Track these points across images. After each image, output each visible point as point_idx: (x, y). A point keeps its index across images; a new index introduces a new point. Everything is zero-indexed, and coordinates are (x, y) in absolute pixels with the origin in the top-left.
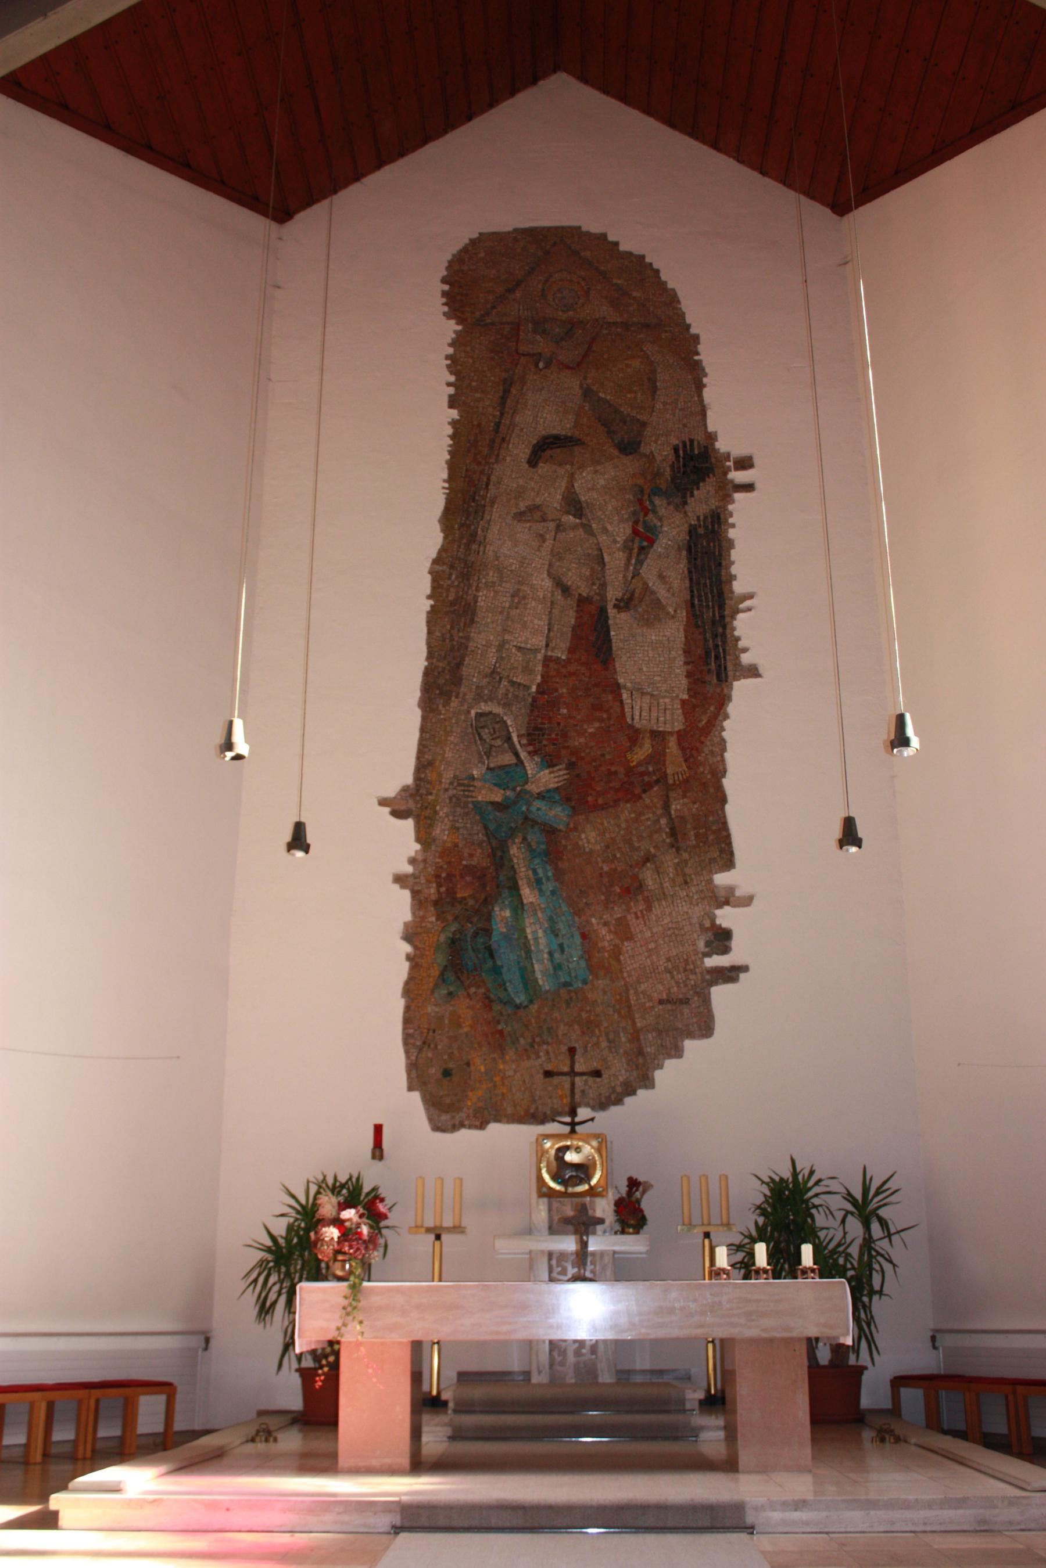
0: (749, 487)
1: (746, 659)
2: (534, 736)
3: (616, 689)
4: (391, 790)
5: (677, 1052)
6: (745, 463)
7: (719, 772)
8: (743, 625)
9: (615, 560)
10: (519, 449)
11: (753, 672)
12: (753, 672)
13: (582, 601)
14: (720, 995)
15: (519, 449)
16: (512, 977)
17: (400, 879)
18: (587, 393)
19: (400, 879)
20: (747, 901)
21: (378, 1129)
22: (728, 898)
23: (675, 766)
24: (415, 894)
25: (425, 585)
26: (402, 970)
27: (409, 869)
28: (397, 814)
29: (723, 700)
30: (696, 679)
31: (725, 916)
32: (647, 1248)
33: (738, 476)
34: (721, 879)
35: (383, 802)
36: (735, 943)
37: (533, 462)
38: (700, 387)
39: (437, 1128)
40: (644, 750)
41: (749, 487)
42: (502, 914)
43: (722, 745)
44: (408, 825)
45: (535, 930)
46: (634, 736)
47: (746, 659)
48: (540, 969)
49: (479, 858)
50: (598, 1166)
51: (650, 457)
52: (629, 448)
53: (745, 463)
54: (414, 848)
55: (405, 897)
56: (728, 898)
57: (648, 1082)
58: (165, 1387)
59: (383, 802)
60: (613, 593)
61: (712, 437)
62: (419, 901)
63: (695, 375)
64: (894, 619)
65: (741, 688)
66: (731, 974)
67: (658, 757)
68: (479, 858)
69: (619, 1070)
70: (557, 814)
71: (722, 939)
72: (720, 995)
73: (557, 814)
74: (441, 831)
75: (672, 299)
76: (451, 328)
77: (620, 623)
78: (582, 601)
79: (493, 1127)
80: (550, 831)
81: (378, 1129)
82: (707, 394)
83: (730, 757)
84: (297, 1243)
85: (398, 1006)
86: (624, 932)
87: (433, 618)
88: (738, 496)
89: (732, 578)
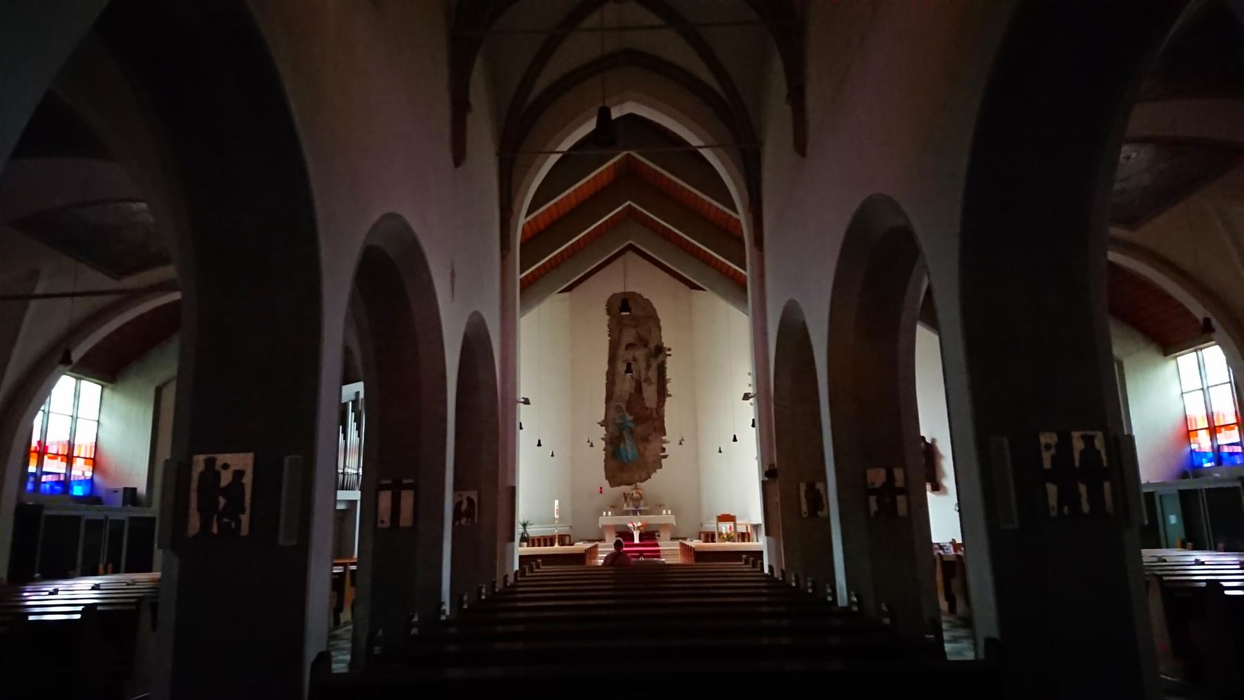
0: (670, 355)
1: (669, 393)
2: (627, 409)
3: (643, 399)
4: (600, 421)
5: (655, 471)
6: (669, 350)
7: (663, 417)
8: (669, 386)
9: (643, 372)
10: (623, 347)
11: (670, 396)
12: (670, 396)
13: (637, 381)
14: (663, 461)
15: (623, 347)
16: (624, 458)
17: (603, 439)
18: (637, 333)
19: (603, 439)
20: (668, 442)
21: (601, 488)
22: (665, 442)
23: (655, 415)
24: (606, 442)
25: (605, 377)
26: (604, 457)
27: (604, 437)
28: (602, 426)
29: (664, 401)
30: (659, 398)
31: (665, 445)
32: (631, 459)
33: (668, 353)
34: (664, 438)
35: (599, 423)
36: (666, 451)
37: (626, 349)
38: (660, 331)
39: (611, 486)
40: (648, 412)
41: (670, 355)
42: (622, 445)
43: (664, 411)
44: (604, 428)
45: (629, 448)
46: (647, 409)
47: (669, 393)
48: (630, 456)
49: (617, 434)
50: (194, 485)
51: (650, 349)
52: (646, 346)
53: (669, 350)
54: (605, 432)
55: (604, 442)
56: (665, 442)
57: (650, 478)
58: (569, 536)
59: (599, 423)
60: (642, 379)
61: (663, 344)
62: (606, 444)
63: (660, 328)
65: (668, 399)
66: (665, 457)
67: (652, 413)
68: (617, 434)
69: (644, 475)
70: (632, 425)
71: (663, 450)
72: (663, 461)
73: (632, 425)
74: (610, 429)
75: (654, 310)
76: (608, 317)
77: (644, 385)
78: (637, 381)
79: (607, 481)
80: (631, 429)
81: (601, 488)
82: (662, 333)
83: (666, 413)
85: (603, 464)
86: (645, 448)
87: (607, 384)
88: (668, 357)
89: (666, 376)
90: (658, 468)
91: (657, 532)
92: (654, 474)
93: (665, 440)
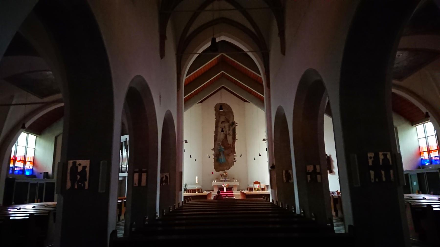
0: (237, 125)
1: (237, 139)
2: (222, 144)
3: (228, 141)
4: (212, 149)
5: (232, 166)
6: (237, 123)
7: (235, 147)
8: (237, 136)
9: (227, 131)
10: (220, 122)
11: (237, 140)
12: (237, 140)
13: (225, 134)
14: (235, 163)
15: (220, 122)
16: (221, 162)
17: (213, 155)
18: (225, 118)
19: (213, 155)
20: (236, 156)
21: (213, 172)
22: (235, 156)
23: (232, 147)
24: (214, 156)
25: (214, 133)
26: (214, 161)
27: (214, 154)
28: (213, 150)
29: (235, 142)
30: (233, 140)
31: (235, 157)
33: (236, 124)
34: (235, 155)
35: (212, 149)
36: (236, 159)
37: (221, 123)
38: (234, 117)
39: (216, 172)
40: (229, 145)
41: (237, 125)
42: (220, 157)
43: (235, 145)
44: (214, 151)
45: (222, 158)
46: (229, 144)
47: (237, 139)
48: (223, 161)
49: (218, 153)
51: (230, 123)
52: (228, 122)
53: (237, 123)
54: (214, 153)
55: (214, 156)
56: (235, 156)
57: (230, 168)
58: (201, 189)
59: (212, 149)
60: (227, 134)
61: (234, 121)
62: (214, 156)
63: (233, 116)
64: (238, 63)
65: (236, 141)
66: (235, 161)
67: (230, 146)
68: (218, 153)
69: (228, 168)
70: (223, 150)
71: (235, 159)
72: (235, 163)
73: (223, 150)
74: (216, 151)
75: (231, 110)
76: (215, 112)
77: (228, 136)
78: (225, 134)
79: (215, 170)
80: (223, 151)
81: (213, 172)
82: (234, 118)
83: (235, 146)
84: (80, 178)
85: (213, 164)
86: (228, 158)
87: (215, 136)
88: (236, 126)
89: (236, 133)
90: (233, 165)
91: (232, 188)
92: (231, 167)
93: (235, 155)
